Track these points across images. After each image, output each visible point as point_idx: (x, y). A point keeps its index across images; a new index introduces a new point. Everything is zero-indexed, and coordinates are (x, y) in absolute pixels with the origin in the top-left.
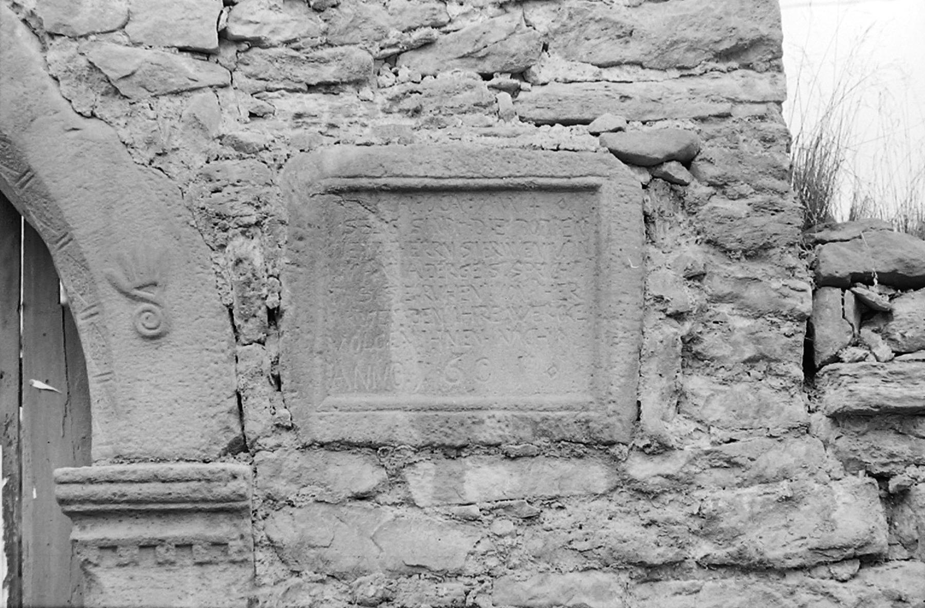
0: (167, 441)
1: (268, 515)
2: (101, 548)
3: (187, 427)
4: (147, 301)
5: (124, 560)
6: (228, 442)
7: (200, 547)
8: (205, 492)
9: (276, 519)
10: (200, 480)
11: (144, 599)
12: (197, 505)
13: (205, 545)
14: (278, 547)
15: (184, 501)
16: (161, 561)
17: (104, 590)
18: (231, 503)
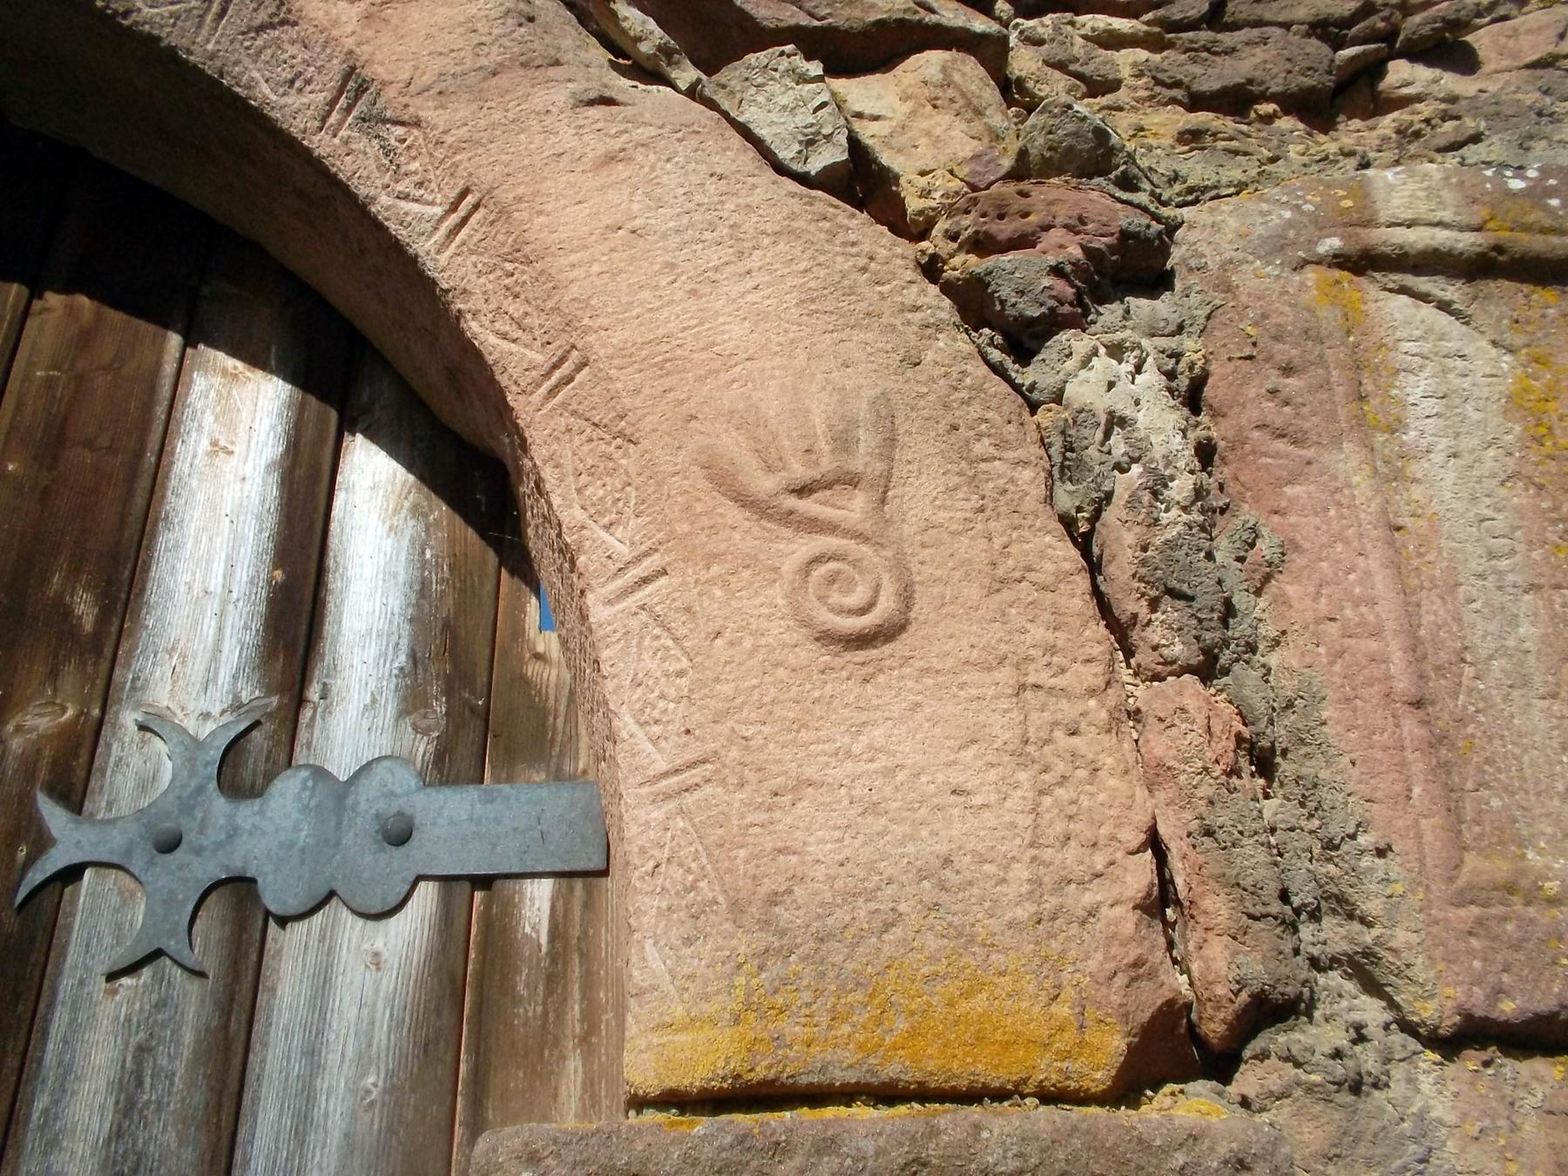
4: (832, 528)
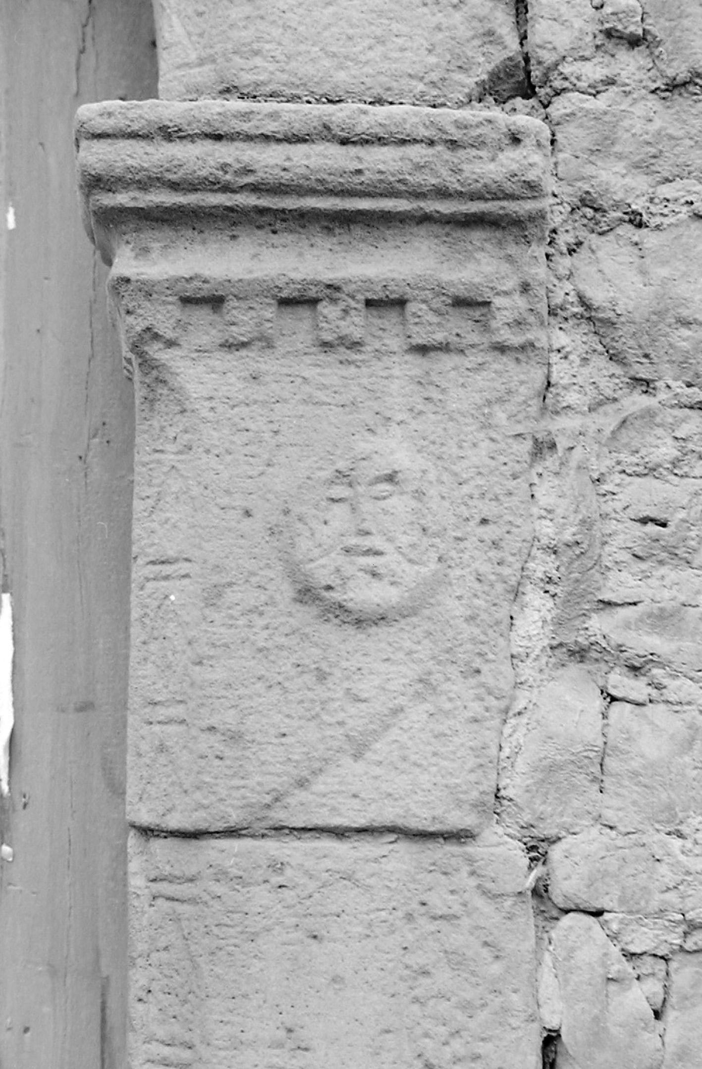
0: (346, 57)
1: (579, 244)
2: (187, 301)
3: (395, 26)
5: (238, 333)
6: (490, 67)
7: (424, 306)
8: (445, 172)
9: (600, 254)
10: (431, 143)
11: (284, 428)
12: (422, 204)
13: (436, 303)
14: (601, 320)
15: (391, 193)
16: (328, 337)
17: (188, 406)
18: (504, 203)
